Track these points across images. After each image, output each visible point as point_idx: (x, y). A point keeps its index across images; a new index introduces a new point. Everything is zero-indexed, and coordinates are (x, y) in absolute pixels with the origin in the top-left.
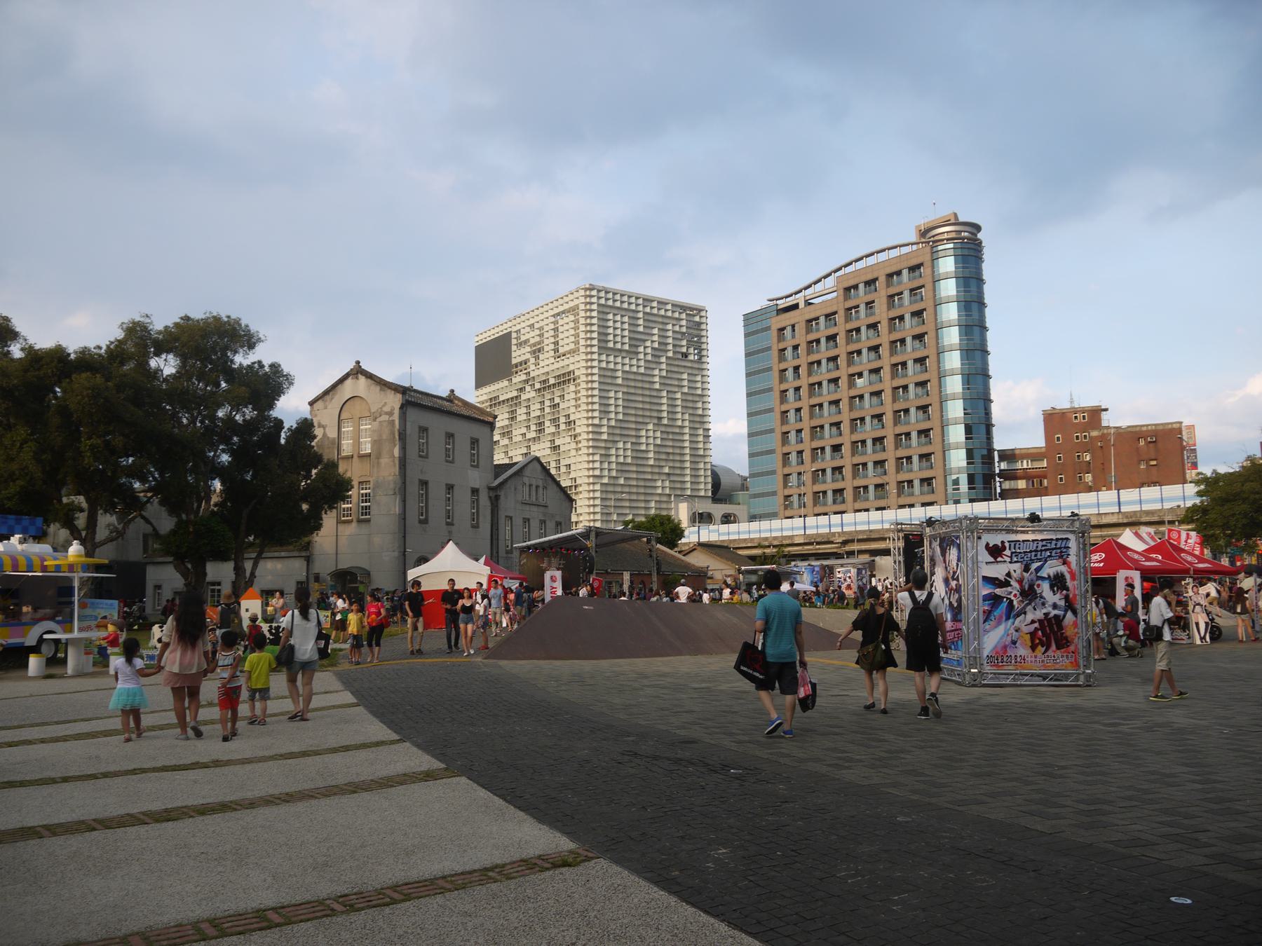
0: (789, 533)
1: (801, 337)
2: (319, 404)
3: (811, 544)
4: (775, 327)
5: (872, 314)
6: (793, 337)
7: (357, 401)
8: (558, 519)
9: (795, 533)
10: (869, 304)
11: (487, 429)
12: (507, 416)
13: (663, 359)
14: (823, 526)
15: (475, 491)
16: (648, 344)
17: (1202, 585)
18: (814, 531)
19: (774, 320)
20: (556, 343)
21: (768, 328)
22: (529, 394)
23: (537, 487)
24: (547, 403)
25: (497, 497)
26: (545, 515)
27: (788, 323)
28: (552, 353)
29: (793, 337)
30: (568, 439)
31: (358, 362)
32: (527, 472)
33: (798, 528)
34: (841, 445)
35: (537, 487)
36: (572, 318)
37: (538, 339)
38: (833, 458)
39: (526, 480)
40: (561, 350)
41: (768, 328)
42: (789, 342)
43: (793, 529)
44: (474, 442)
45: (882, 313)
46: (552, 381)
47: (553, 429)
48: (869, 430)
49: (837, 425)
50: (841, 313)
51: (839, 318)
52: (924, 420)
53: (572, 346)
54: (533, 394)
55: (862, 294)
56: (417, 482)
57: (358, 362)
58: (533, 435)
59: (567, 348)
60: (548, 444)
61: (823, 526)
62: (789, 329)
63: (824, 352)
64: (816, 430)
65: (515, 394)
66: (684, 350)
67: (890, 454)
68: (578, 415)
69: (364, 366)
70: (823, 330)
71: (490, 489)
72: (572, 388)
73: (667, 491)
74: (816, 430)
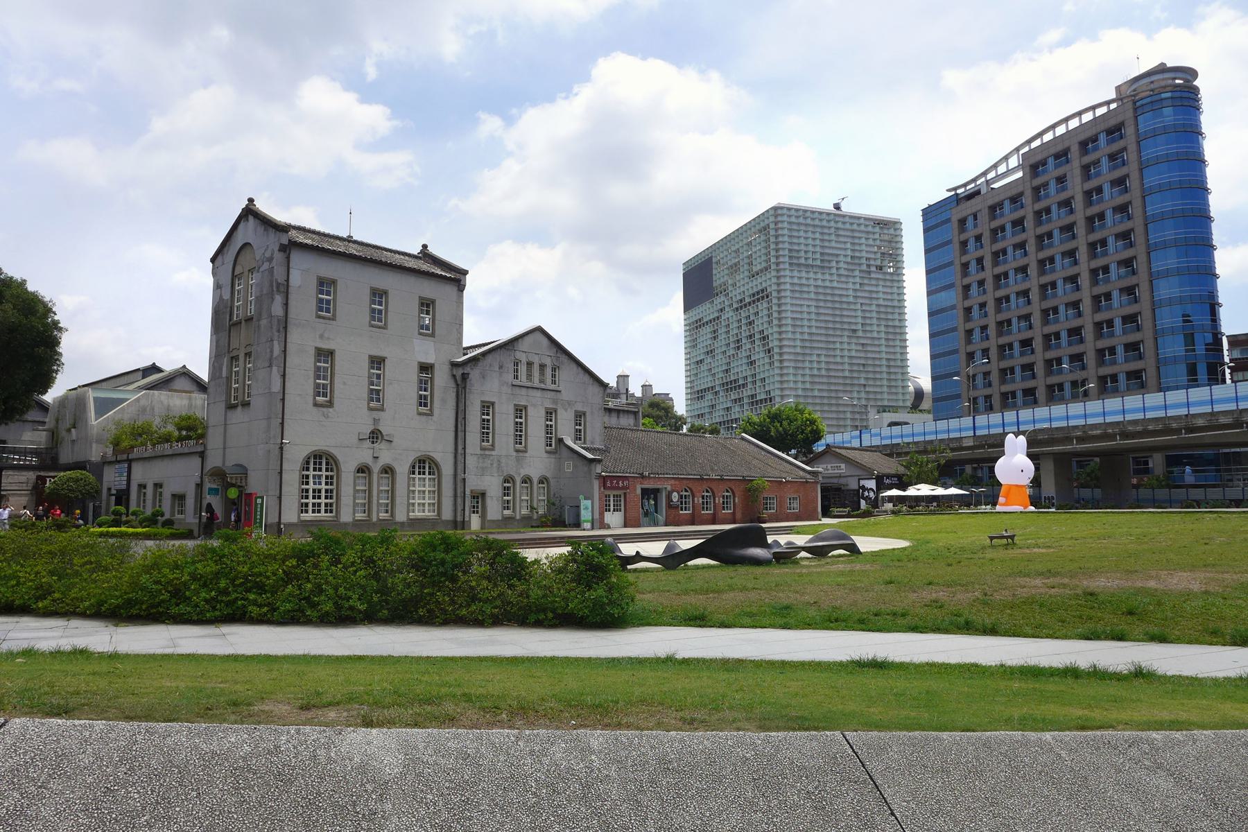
0: (957, 435)
1: (985, 226)
2: (219, 258)
3: (982, 447)
4: (955, 219)
5: (1064, 189)
6: (975, 226)
7: (247, 251)
8: (580, 408)
9: (964, 434)
10: (1061, 180)
11: (450, 289)
12: (709, 336)
13: (857, 273)
14: (996, 426)
15: (425, 368)
16: (841, 258)
17: (590, 588)
18: (985, 432)
19: (954, 211)
20: (750, 264)
21: (948, 220)
22: (729, 314)
23: (542, 367)
24: (744, 321)
25: (465, 377)
26: (555, 401)
27: (969, 212)
28: (747, 273)
29: (975, 226)
30: (762, 355)
31: (251, 200)
32: (524, 345)
33: (966, 429)
34: (1032, 339)
35: (542, 367)
36: (763, 238)
37: (734, 261)
38: (1022, 354)
39: (523, 358)
40: (755, 269)
41: (948, 220)
42: (971, 233)
43: (960, 430)
44: (427, 305)
45: (1076, 187)
46: (747, 300)
47: (749, 346)
48: (1064, 321)
49: (1027, 317)
50: (1028, 193)
51: (1027, 199)
52: (1130, 303)
53: (764, 265)
54: (731, 314)
55: (1052, 172)
56: (312, 352)
57: (251, 200)
58: (732, 352)
59: (759, 267)
60: (745, 361)
61: (996, 426)
62: (971, 219)
63: (1009, 240)
64: (1004, 326)
65: (716, 315)
66: (878, 262)
67: (1090, 346)
68: (770, 331)
69: (262, 206)
70: (1008, 215)
71: (454, 365)
72: (765, 305)
73: (864, 402)
74: (1004, 326)
